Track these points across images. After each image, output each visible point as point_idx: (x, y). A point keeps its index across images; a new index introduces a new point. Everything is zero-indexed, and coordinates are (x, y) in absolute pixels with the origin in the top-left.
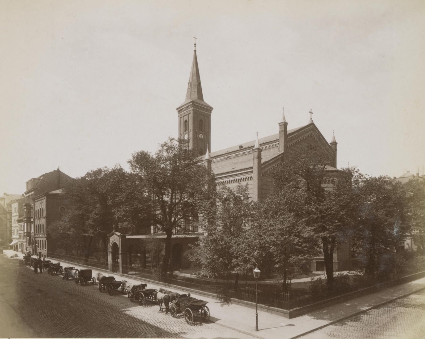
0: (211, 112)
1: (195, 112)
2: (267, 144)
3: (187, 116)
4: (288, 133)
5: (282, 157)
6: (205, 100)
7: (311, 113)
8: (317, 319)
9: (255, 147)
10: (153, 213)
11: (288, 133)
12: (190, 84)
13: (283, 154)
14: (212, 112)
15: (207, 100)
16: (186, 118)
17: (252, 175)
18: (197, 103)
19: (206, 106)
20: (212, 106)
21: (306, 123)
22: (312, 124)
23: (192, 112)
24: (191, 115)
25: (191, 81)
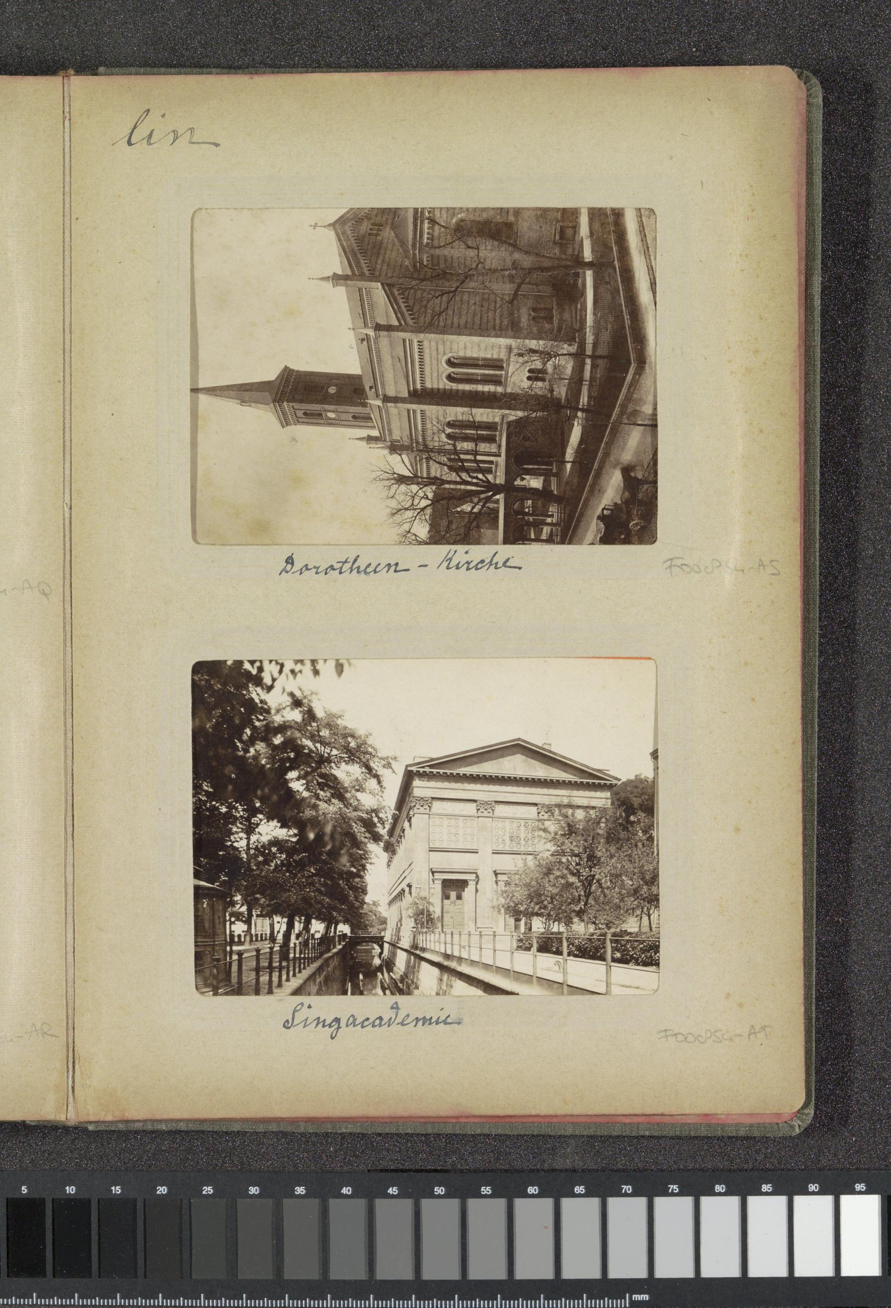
0: (293, 370)
1: (293, 400)
2: (363, 308)
3: (297, 412)
4: (350, 273)
5: (388, 285)
6: (273, 379)
7: (315, 226)
8: (24, 1122)
9: (381, 405)
10: (297, 918)
11: (350, 273)
12: (243, 402)
13: (382, 284)
14: (291, 367)
15: (271, 374)
16: (300, 414)
17: (415, 340)
18: (277, 394)
19: (282, 378)
20: (282, 367)
21: (331, 234)
22: (333, 225)
23: (291, 404)
24: (296, 405)
25: (239, 402)
